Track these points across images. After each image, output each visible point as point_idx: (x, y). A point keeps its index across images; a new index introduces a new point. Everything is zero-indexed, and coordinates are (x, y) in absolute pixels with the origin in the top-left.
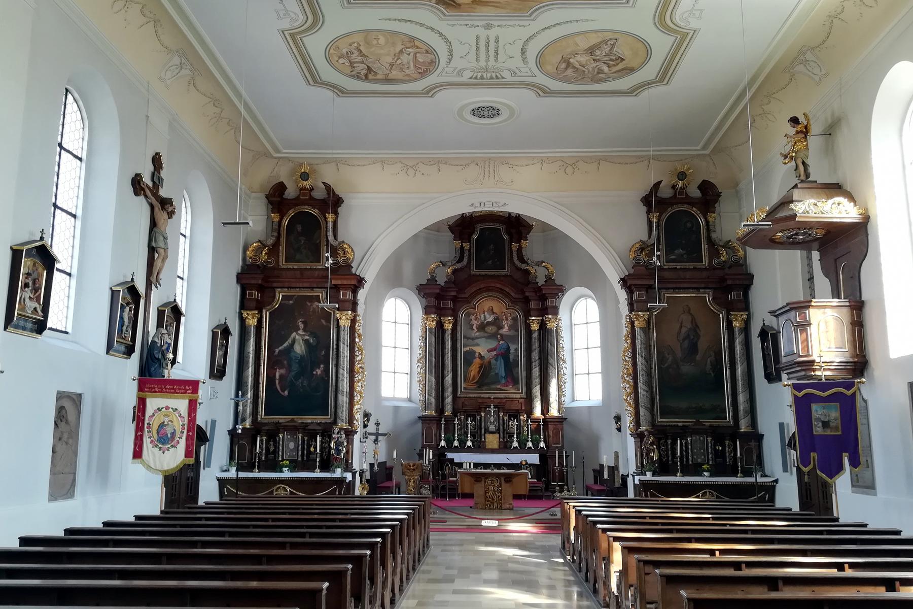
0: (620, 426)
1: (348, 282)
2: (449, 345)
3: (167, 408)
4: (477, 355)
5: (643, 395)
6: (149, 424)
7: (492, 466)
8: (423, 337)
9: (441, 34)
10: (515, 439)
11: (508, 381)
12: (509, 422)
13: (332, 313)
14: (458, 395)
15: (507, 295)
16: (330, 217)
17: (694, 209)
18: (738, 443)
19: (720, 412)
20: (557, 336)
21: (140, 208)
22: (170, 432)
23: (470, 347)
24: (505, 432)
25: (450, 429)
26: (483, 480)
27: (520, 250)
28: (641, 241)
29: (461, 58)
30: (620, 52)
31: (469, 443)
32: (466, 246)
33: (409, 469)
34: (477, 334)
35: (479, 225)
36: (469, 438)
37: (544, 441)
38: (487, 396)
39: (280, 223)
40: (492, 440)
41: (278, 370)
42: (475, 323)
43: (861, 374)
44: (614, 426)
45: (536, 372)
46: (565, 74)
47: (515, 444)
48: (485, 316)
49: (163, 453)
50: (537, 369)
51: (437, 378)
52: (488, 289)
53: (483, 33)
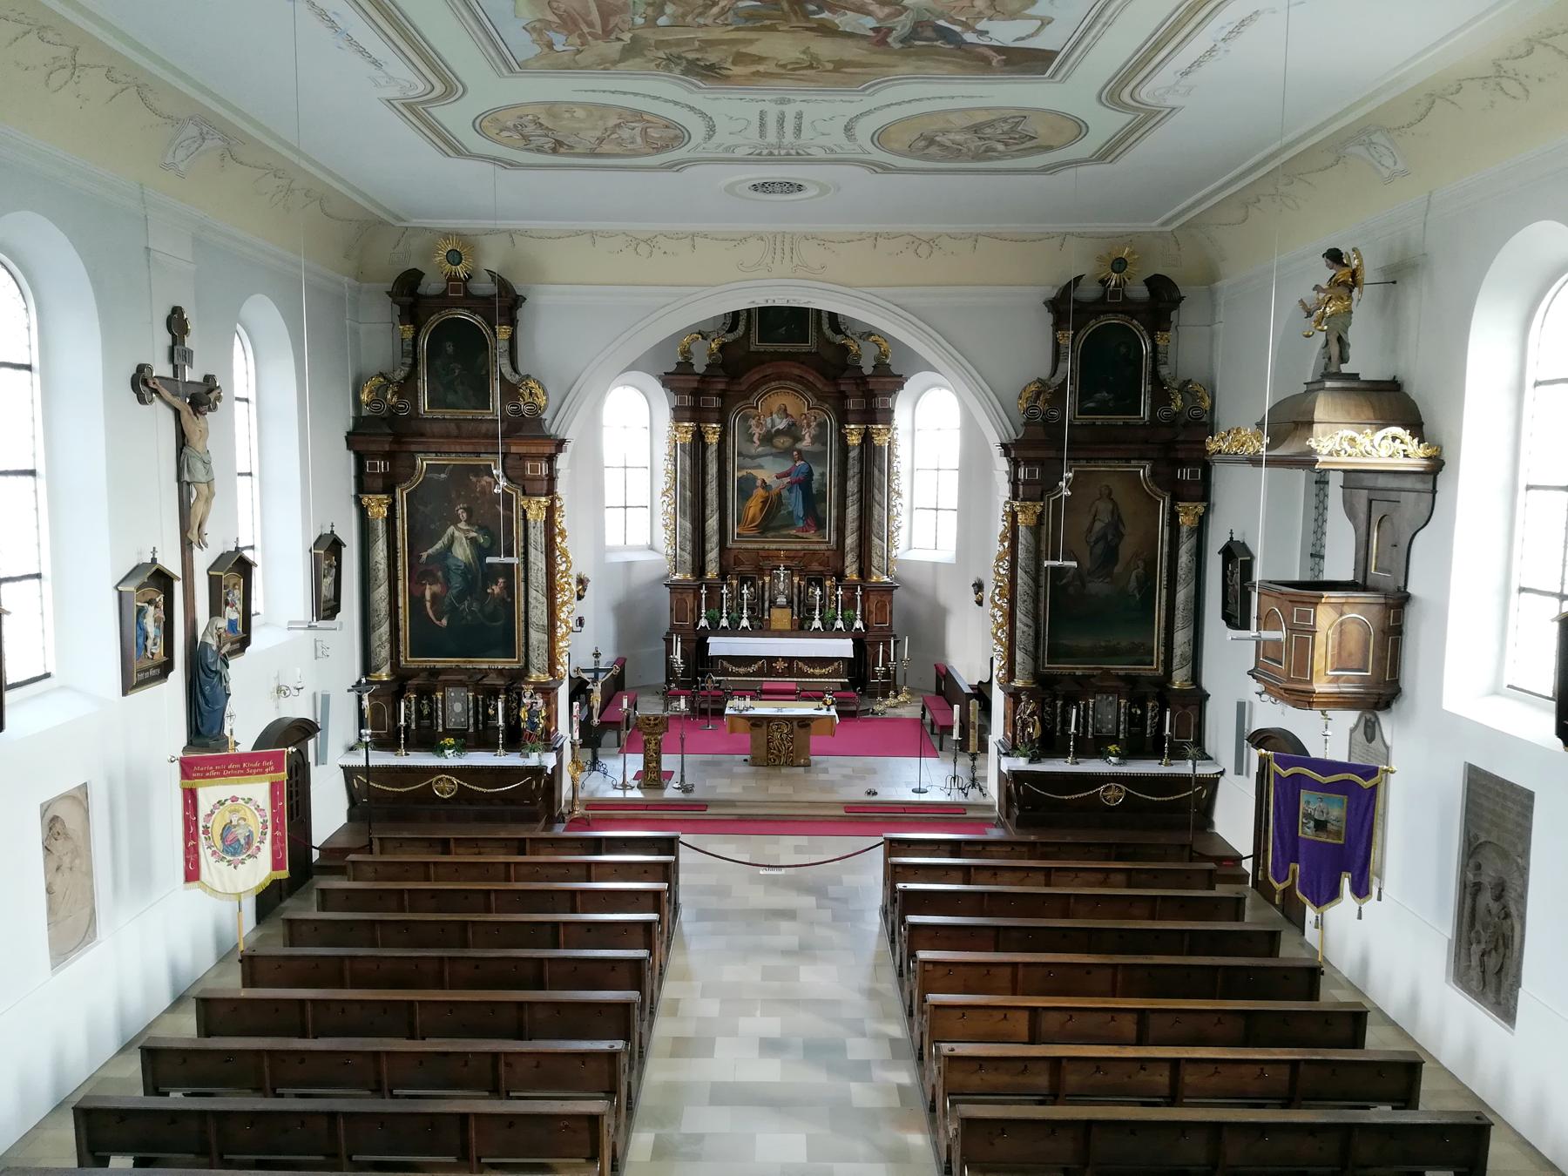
1: (541, 450)
2: (713, 469)
3: (234, 799)
4: (759, 483)
5: (1023, 632)
6: (206, 827)
7: (780, 659)
8: (670, 456)
9: (692, 109)
10: (817, 617)
11: (809, 525)
13: (514, 496)
15: (810, 386)
16: (503, 332)
17: (1135, 322)
18: (1168, 713)
19: (1142, 653)
20: (889, 455)
21: (158, 420)
22: (243, 835)
23: (749, 471)
25: (714, 602)
28: (1039, 380)
29: (730, 134)
30: (1031, 130)
31: (745, 623)
34: (760, 449)
36: (745, 615)
37: (861, 619)
38: (773, 546)
39: (415, 339)
40: (781, 618)
41: (428, 586)
42: (757, 432)
43: (1387, 706)
44: (973, 597)
46: (925, 152)
47: (817, 624)
48: (772, 420)
49: (235, 867)
51: (693, 522)
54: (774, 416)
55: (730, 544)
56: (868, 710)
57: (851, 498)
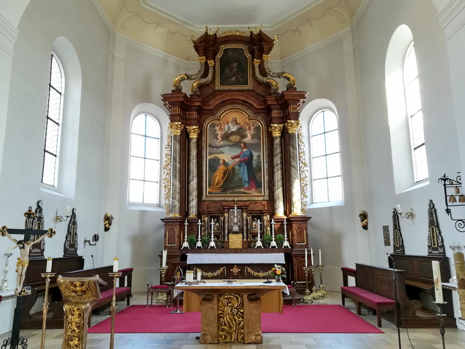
0: (367, 224)
2: (194, 152)
4: (221, 162)
8: (169, 145)
10: (259, 239)
11: (251, 186)
12: (252, 223)
14: (203, 199)
15: (250, 106)
23: (215, 155)
24: (249, 232)
26: (216, 298)
27: (262, 62)
31: (212, 244)
32: (211, 63)
33: (76, 292)
34: (222, 143)
35: (223, 46)
36: (212, 239)
37: (287, 240)
38: (231, 199)
45: (278, 175)
47: (259, 244)
48: (229, 127)
50: (280, 172)
52: (232, 102)
54: (230, 124)
55: (204, 197)
56: (300, 299)
57: (276, 167)
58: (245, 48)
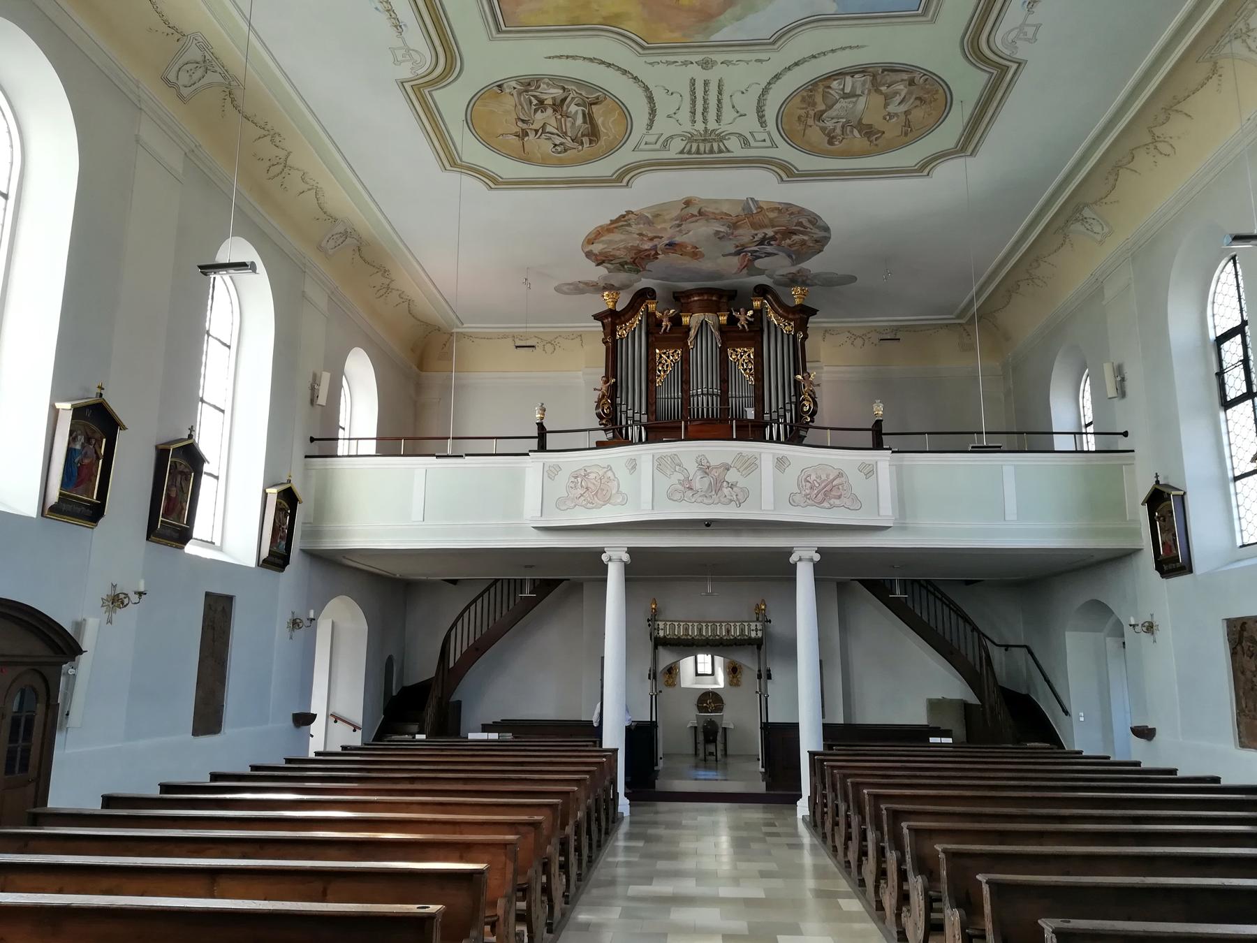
53: (700, 74)
58: (857, 786)
